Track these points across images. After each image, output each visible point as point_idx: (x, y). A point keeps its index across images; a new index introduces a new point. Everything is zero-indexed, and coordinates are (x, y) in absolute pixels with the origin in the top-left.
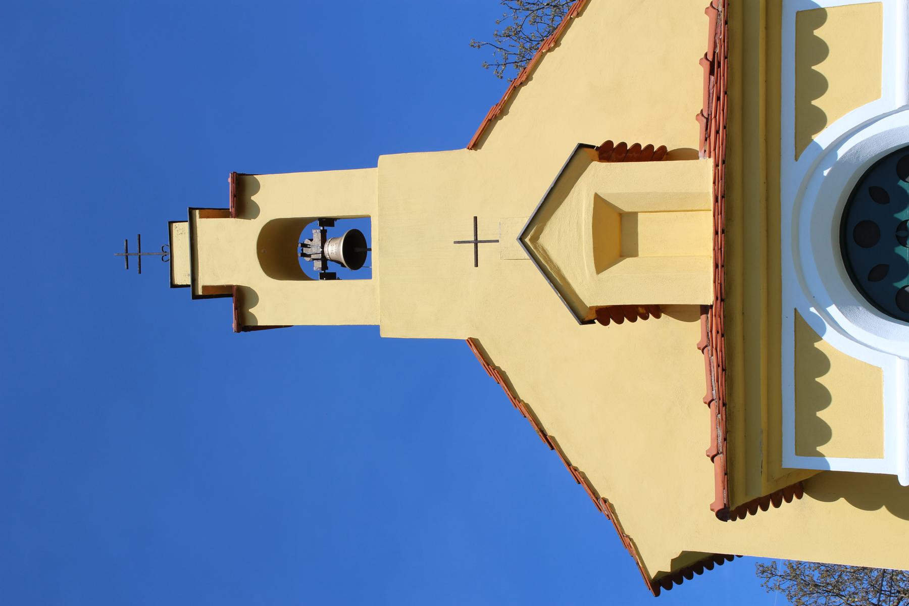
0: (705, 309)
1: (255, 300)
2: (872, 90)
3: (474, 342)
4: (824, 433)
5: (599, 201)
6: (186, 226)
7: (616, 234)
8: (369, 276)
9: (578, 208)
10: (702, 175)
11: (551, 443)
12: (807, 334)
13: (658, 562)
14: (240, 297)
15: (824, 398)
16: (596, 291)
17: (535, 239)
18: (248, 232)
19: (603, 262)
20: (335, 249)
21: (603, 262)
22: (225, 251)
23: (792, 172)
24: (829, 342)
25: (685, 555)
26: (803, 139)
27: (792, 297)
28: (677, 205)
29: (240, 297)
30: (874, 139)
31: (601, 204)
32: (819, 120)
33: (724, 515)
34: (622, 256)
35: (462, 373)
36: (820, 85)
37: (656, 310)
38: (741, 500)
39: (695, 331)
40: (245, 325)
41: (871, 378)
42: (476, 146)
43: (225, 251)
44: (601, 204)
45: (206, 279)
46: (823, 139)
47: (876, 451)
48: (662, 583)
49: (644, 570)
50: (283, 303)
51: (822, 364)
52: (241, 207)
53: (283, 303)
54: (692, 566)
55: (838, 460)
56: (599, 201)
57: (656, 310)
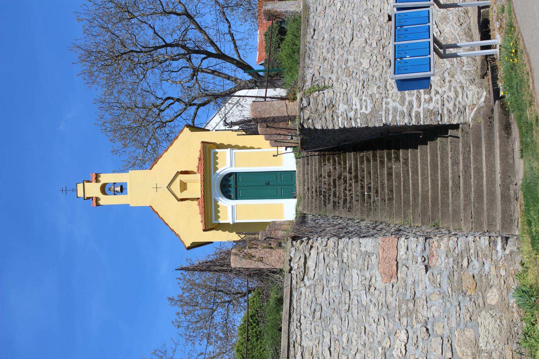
0: (198, 199)
1: (99, 199)
2: (225, 164)
3: (151, 206)
4: (219, 217)
5: (181, 181)
6: (82, 184)
7: (183, 186)
8: (127, 194)
9: (177, 183)
10: (198, 177)
11: (167, 224)
12: (216, 202)
13: (188, 244)
14: (97, 199)
15: (219, 212)
16: (180, 197)
17: (171, 187)
18: (99, 185)
19: (182, 191)
20: (118, 189)
21: (182, 191)
22: (93, 190)
23: (213, 177)
24: (220, 203)
25: (193, 243)
26: (215, 172)
27: (213, 196)
28: (194, 181)
29: (97, 199)
30: (223, 174)
31: (181, 181)
32: (217, 169)
33: (204, 231)
34: (184, 190)
35: (149, 213)
36: (217, 163)
37: (187, 199)
38: (207, 228)
39: (196, 203)
40: (98, 205)
41: (226, 208)
42: (151, 169)
43: (93, 190)
44: (181, 181)
45: (87, 196)
46: (218, 172)
47: (227, 219)
48: (189, 248)
49: (185, 246)
50: (106, 200)
51: (218, 206)
52: (97, 181)
53: (106, 200)
54: (195, 245)
55: (221, 221)
56: (181, 181)
57: (187, 199)
